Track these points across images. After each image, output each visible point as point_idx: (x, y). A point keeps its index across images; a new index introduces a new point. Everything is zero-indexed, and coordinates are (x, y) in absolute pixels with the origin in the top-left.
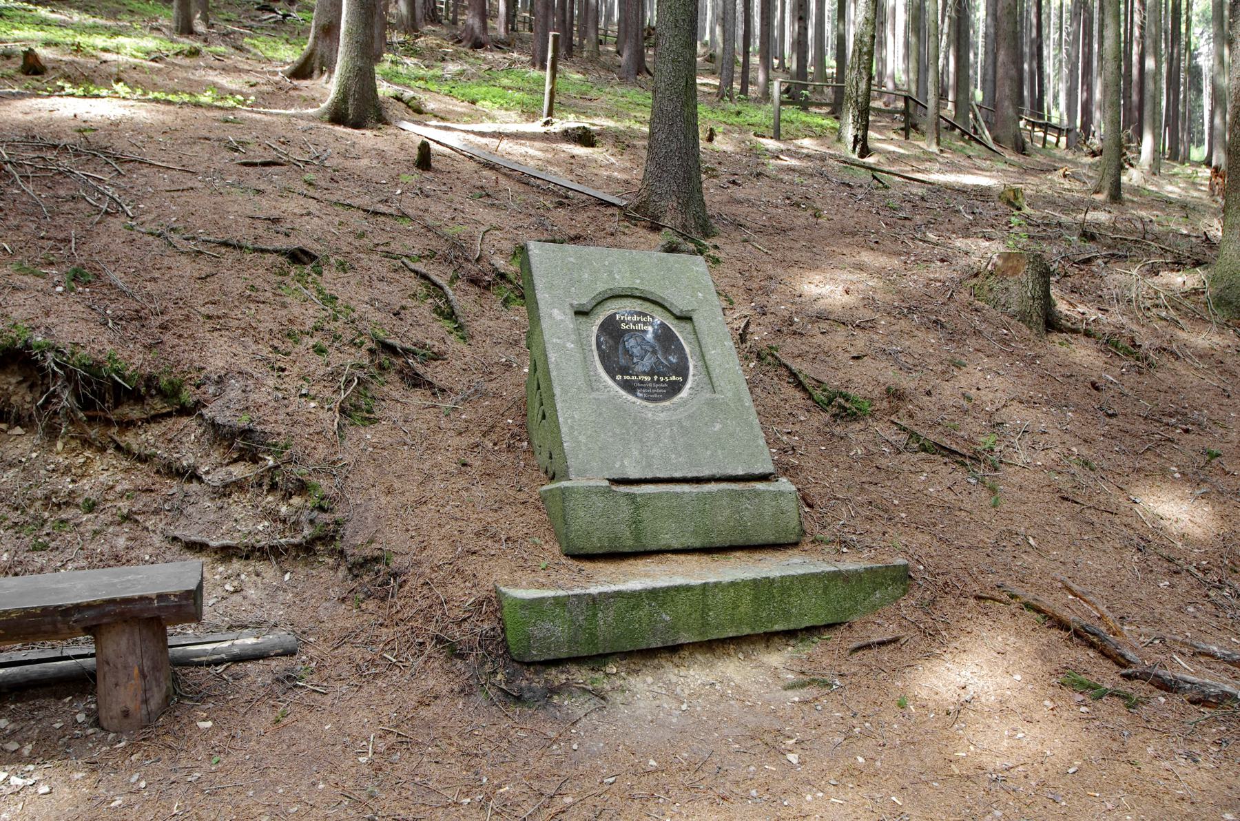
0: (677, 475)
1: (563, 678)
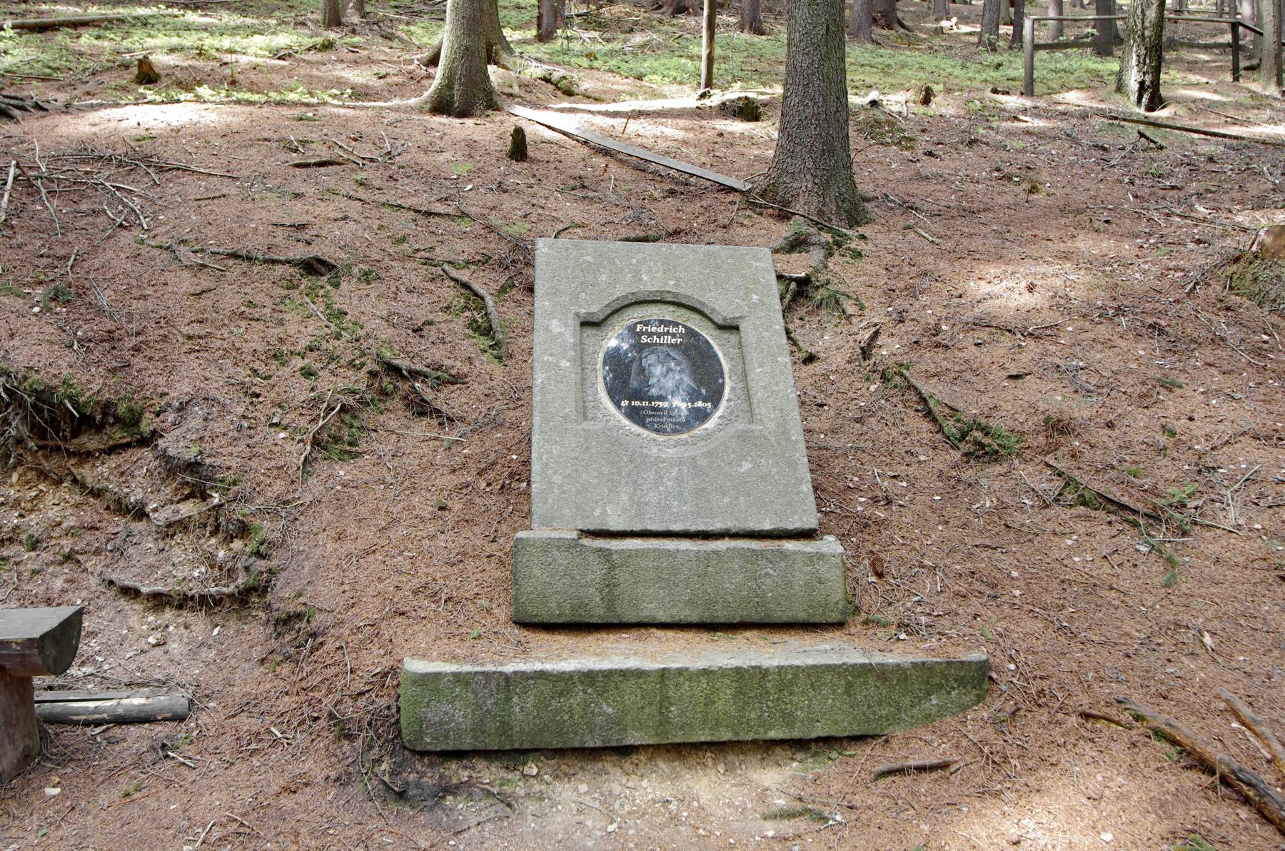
0: (676, 527)
1: (464, 775)
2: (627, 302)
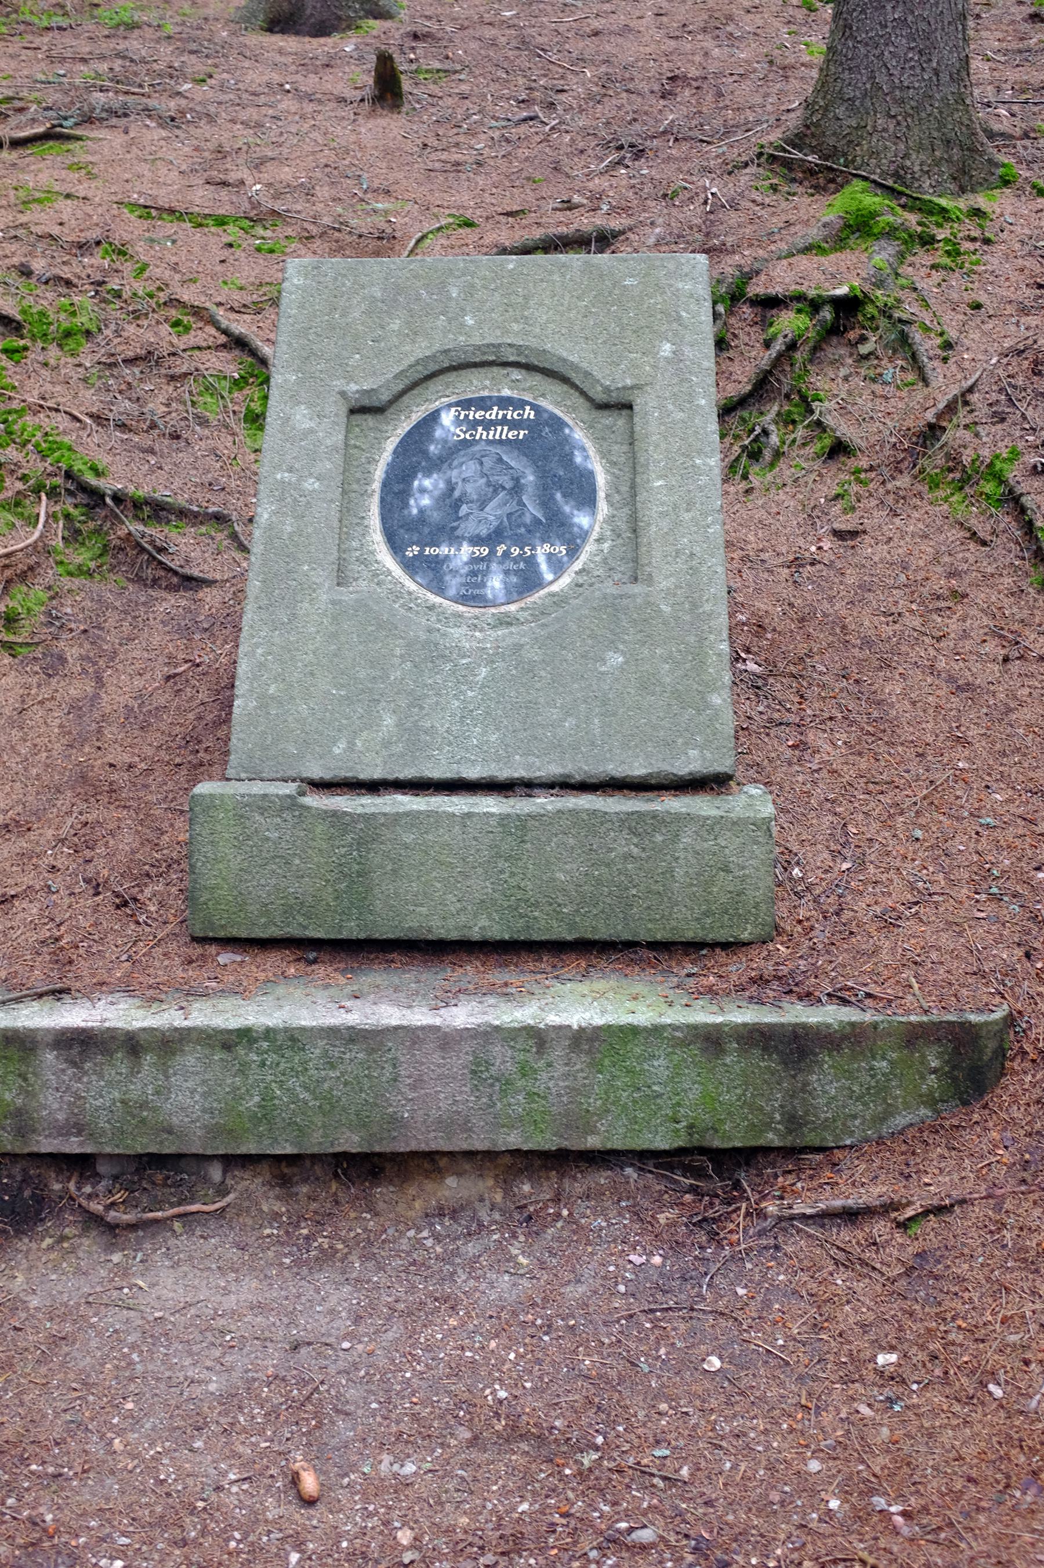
0: (472, 773)
2: (433, 367)
